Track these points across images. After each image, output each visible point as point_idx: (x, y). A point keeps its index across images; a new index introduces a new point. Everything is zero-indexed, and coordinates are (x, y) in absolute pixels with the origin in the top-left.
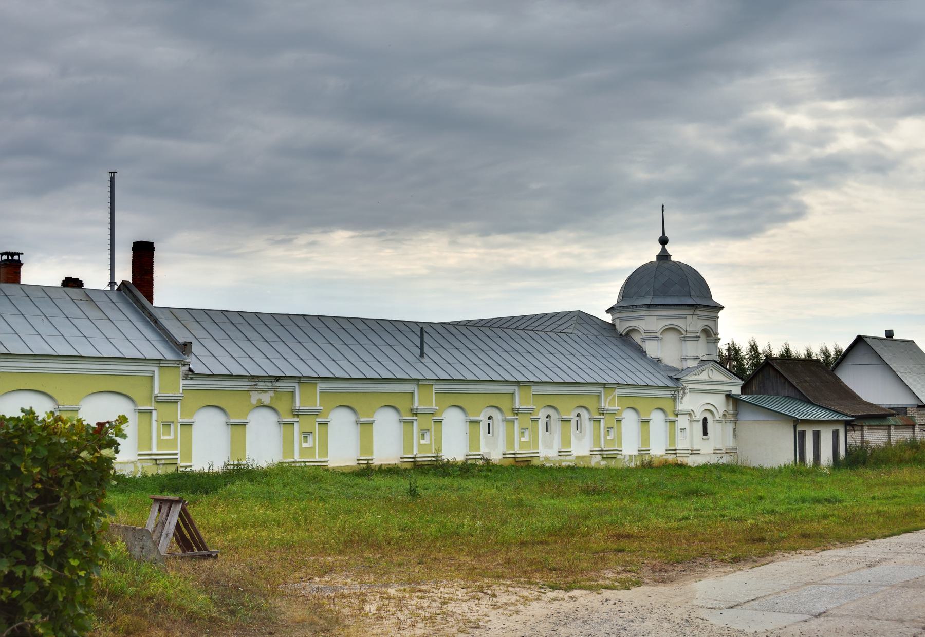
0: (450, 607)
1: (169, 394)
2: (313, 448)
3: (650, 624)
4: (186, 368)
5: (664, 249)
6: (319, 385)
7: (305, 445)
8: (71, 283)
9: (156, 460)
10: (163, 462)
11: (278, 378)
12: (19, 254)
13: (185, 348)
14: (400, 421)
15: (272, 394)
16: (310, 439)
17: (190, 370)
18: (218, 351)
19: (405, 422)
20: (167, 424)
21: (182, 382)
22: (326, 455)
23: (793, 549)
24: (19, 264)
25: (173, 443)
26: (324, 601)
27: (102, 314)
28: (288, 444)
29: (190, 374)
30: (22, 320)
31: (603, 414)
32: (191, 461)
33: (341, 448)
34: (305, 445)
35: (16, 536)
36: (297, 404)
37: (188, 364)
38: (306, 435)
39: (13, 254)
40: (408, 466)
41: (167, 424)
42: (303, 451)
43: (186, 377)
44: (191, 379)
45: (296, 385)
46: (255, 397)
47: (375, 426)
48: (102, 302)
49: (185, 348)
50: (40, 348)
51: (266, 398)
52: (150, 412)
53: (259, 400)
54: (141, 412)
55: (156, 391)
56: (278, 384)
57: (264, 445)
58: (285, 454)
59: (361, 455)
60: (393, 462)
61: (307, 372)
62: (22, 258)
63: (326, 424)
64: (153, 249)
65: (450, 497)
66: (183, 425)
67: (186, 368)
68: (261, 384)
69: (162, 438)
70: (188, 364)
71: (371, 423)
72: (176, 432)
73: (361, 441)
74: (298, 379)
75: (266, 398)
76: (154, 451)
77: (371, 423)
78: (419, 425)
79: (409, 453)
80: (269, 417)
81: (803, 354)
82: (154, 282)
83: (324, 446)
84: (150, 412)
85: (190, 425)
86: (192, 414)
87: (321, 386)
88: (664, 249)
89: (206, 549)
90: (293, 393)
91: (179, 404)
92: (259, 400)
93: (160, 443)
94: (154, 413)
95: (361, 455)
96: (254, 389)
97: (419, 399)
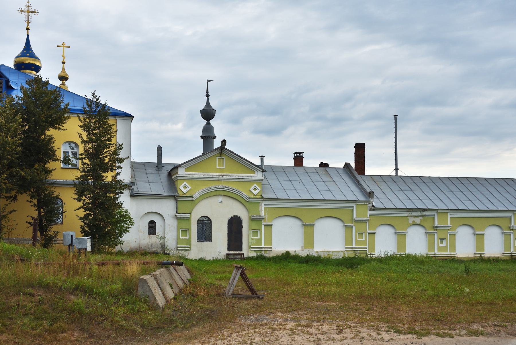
0: (85, 138)
1: (362, 218)
2: (446, 247)
3: (406, 300)
4: (371, 205)
5: (208, 124)
6: (449, 214)
7: (441, 245)
8: (324, 165)
9: (355, 251)
10: (359, 252)
11: (424, 210)
12: (302, 153)
13: (370, 194)
14: (426, 233)
15: (422, 218)
16: (444, 242)
17: (373, 206)
18: (471, 197)
19: (505, 234)
20: (361, 233)
21: (369, 212)
22: (455, 251)
23: (466, 260)
24: (302, 158)
25: (364, 243)
26: (283, 333)
27: (378, 187)
28: (431, 245)
29: (373, 208)
30: (404, 184)
31: (437, 230)
32: (242, 250)
33: (464, 247)
34: (441, 245)
35: (103, 159)
36: (436, 223)
37: (372, 203)
38: (442, 240)
39: (300, 153)
40: (508, 258)
41: (361, 233)
42: (440, 249)
43: (371, 209)
44: (374, 210)
45: (436, 214)
46: (411, 220)
47: (485, 236)
48: (340, 172)
49: (370, 194)
50: (293, 195)
51: (418, 220)
52: (352, 227)
53: (414, 221)
54: (346, 227)
55: (355, 217)
56: (424, 213)
57: (417, 244)
58: (429, 250)
59: (476, 251)
60: (497, 256)
61: (442, 206)
62: (304, 155)
63: (455, 234)
64: (364, 146)
65: (462, 292)
66: (369, 234)
67: (371, 205)
68: (414, 213)
69: (358, 240)
70: (372, 203)
71: (483, 234)
72: (446, 243)
73: (476, 241)
74: (436, 210)
75: (418, 220)
76: (354, 246)
77: (483, 234)
78: (514, 236)
79: (508, 251)
80: (420, 231)
81: (212, 259)
82: (227, 238)
83: (453, 246)
84: (352, 227)
85: (374, 234)
86: (375, 229)
87: (450, 214)
88: (208, 124)
89: (256, 294)
90: (434, 218)
91: (367, 224)
92: (414, 221)
93: (357, 242)
94: (354, 228)
95: (476, 251)
96: (410, 215)
97: (438, 220)
